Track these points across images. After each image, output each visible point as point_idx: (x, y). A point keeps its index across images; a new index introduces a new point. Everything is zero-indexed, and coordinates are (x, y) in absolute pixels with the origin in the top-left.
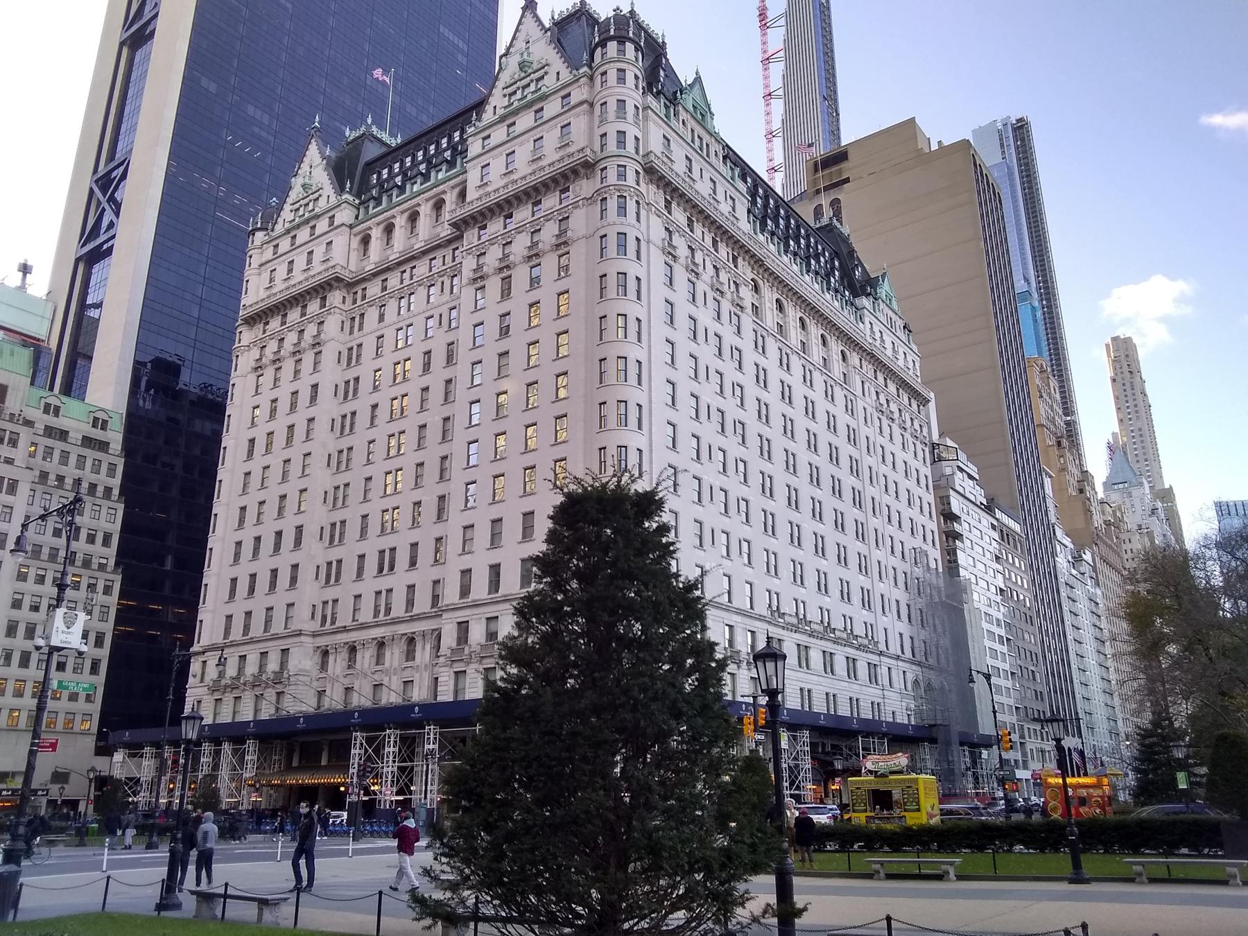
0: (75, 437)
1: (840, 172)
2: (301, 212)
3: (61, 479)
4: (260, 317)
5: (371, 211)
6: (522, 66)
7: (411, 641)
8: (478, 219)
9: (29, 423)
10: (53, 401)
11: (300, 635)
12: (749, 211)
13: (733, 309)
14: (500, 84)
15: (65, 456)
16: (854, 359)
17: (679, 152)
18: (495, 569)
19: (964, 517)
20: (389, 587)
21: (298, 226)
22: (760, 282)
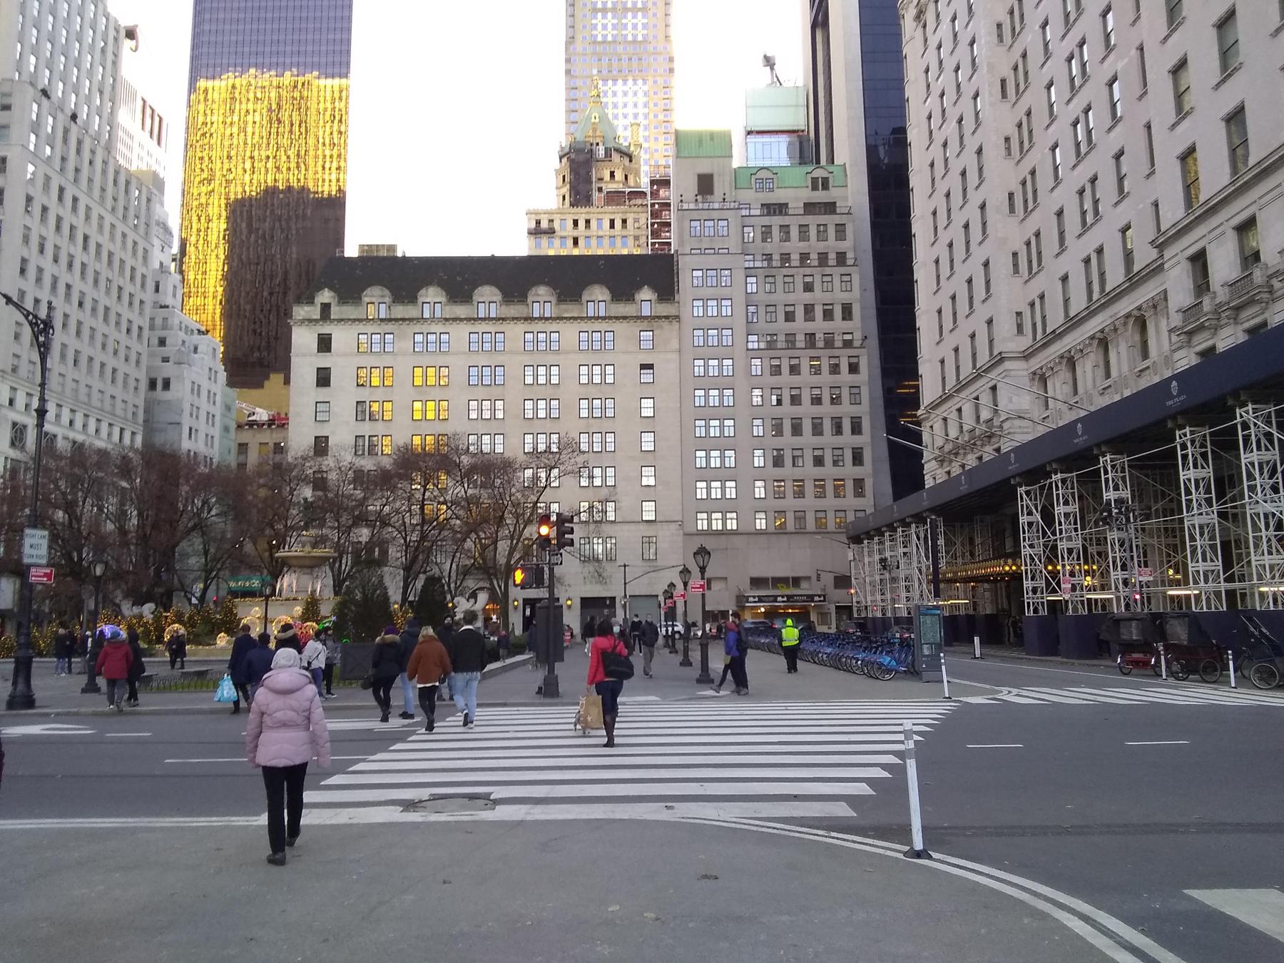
0: (796, 206)
3: (785, 258)
7: (1142, 324)
10: (819, 173)
11: (1002, 360)
15: (785, 229)
20: (1096, 245)
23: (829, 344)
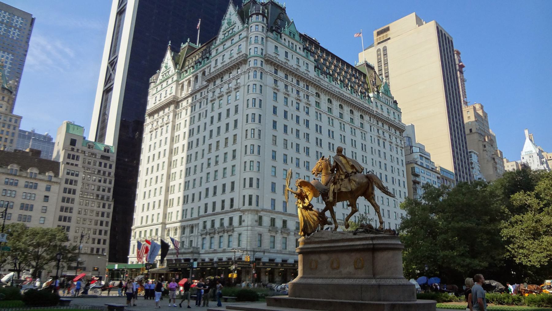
1: (387, 35)
2: (226, 35)
4: (152, 114)
5: (199, 67)
6: (229, 23)
7: (192, 227)
8: (212, 80)
9: (84, 152)
12: (315, 67)
13: (305, 106)
14: (222, 30)
16: (367, 118)
17: (282, 51)
18: (214, 203)
19: (421, 174)
21: (226, 40)
22: (320, 93)
23: (103, 198)
